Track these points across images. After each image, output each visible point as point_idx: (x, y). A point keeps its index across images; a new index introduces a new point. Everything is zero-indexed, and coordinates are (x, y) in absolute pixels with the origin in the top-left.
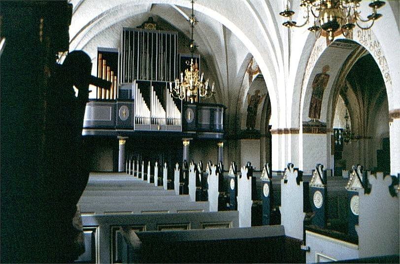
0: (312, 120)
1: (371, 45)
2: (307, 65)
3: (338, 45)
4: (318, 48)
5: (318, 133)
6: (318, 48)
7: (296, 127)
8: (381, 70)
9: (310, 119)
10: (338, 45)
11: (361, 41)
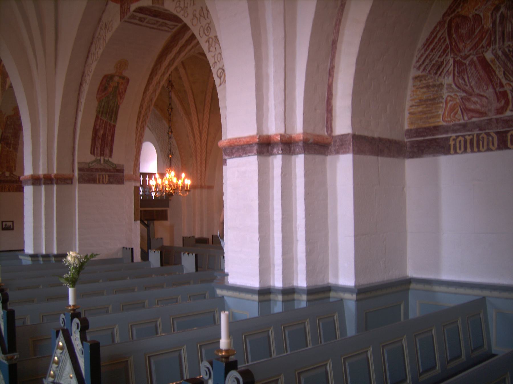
0: (96, 160)
1: (194, 16)
2: (88, 57)
3: (141, 19)
4: (106, 25)
5: (110, 182)
6: (106, 25)
7: (66, 172)
8: (211, 63)
9: (93, 158)
10: (141, 19)
11: (179, 9)
